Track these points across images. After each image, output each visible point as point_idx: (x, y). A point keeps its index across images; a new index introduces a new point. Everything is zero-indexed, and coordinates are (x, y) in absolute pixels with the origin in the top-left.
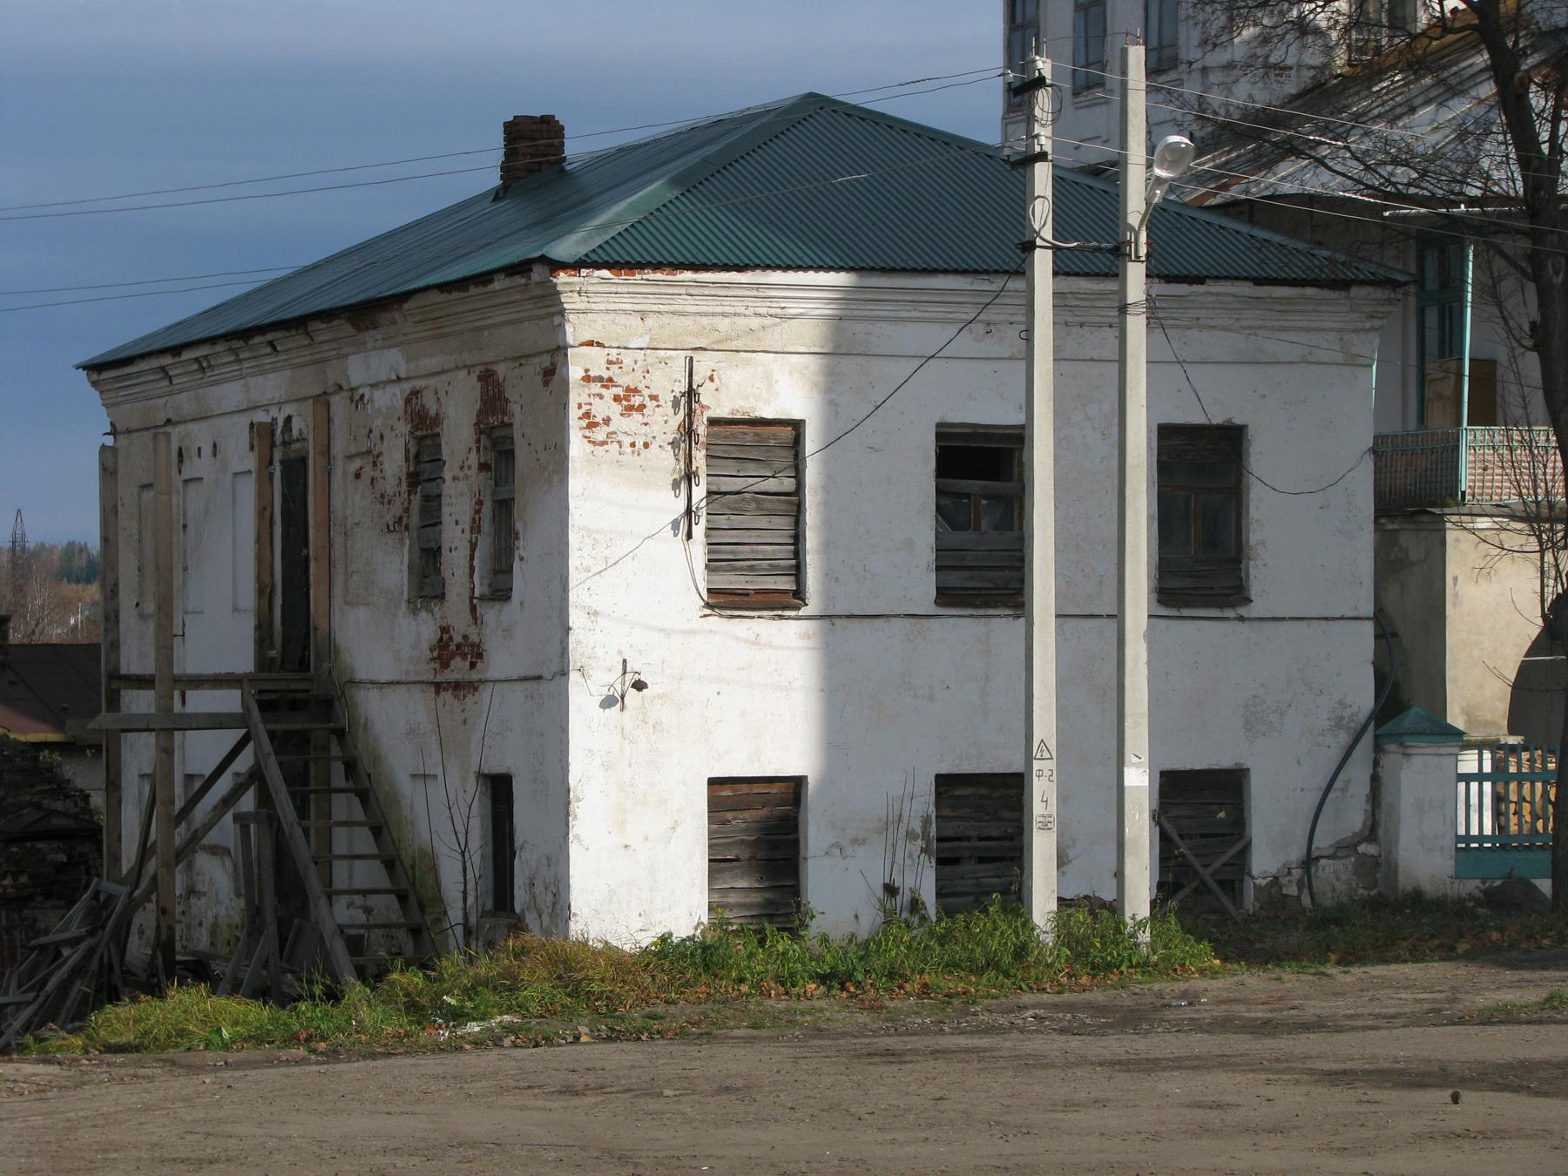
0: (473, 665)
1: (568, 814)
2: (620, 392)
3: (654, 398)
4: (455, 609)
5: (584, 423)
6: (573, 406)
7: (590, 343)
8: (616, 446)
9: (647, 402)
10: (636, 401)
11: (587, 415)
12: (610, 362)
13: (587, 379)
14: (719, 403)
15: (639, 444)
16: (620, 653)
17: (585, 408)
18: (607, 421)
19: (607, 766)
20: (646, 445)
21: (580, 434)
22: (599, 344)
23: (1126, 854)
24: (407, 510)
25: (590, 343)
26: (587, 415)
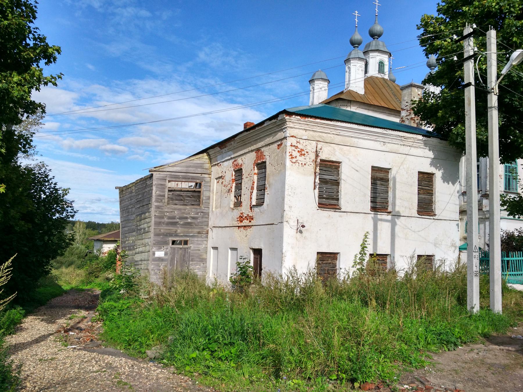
0: (250, 221)
1: (282, 260)
2: (299, 150)
3: (307, 152)
4: (245, 209)
5: (290, 157)
6: (288, 152)
7: (293, 136)
8: (298, 164)
9: (306, 153)
10: (303, 153)
11: (291, 155)
12: (297, 142)
13: (291, 146)
14: (324, 156)
15: (303, 164)
16: (297, 218)
17: (291, 153)
18: (296, 157)
19: (292, 248)
20: (305, 164)
21: (289, 160)
22: (295, 137)
23: (495, 284)
24: (231, 187)
25: (293, 136)
26: (291, 155)
